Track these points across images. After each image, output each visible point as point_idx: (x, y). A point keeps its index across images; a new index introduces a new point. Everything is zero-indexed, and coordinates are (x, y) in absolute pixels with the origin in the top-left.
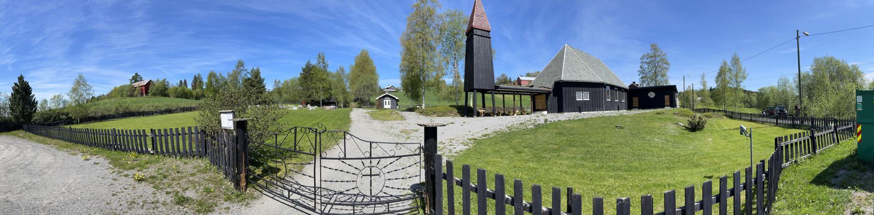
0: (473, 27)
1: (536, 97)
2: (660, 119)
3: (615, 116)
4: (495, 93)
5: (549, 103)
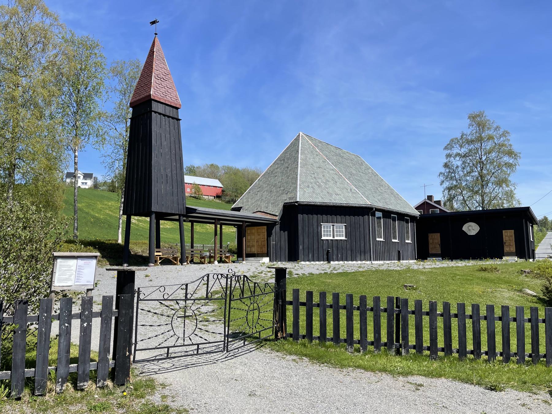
0: (152, 97)
1: (248, 231)
2: (486, 280)
3: (399, 271)
4: (184, 221)
5: (273, 243)
